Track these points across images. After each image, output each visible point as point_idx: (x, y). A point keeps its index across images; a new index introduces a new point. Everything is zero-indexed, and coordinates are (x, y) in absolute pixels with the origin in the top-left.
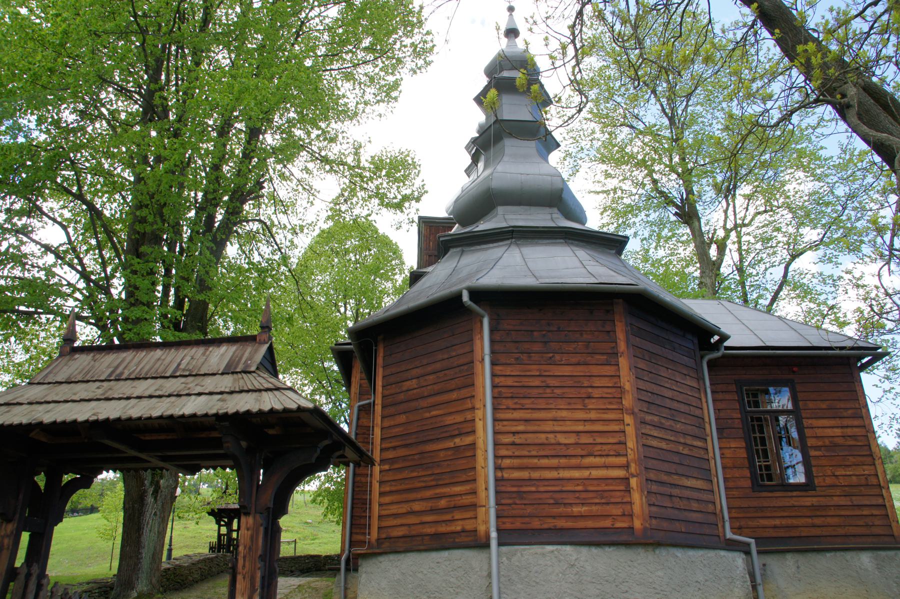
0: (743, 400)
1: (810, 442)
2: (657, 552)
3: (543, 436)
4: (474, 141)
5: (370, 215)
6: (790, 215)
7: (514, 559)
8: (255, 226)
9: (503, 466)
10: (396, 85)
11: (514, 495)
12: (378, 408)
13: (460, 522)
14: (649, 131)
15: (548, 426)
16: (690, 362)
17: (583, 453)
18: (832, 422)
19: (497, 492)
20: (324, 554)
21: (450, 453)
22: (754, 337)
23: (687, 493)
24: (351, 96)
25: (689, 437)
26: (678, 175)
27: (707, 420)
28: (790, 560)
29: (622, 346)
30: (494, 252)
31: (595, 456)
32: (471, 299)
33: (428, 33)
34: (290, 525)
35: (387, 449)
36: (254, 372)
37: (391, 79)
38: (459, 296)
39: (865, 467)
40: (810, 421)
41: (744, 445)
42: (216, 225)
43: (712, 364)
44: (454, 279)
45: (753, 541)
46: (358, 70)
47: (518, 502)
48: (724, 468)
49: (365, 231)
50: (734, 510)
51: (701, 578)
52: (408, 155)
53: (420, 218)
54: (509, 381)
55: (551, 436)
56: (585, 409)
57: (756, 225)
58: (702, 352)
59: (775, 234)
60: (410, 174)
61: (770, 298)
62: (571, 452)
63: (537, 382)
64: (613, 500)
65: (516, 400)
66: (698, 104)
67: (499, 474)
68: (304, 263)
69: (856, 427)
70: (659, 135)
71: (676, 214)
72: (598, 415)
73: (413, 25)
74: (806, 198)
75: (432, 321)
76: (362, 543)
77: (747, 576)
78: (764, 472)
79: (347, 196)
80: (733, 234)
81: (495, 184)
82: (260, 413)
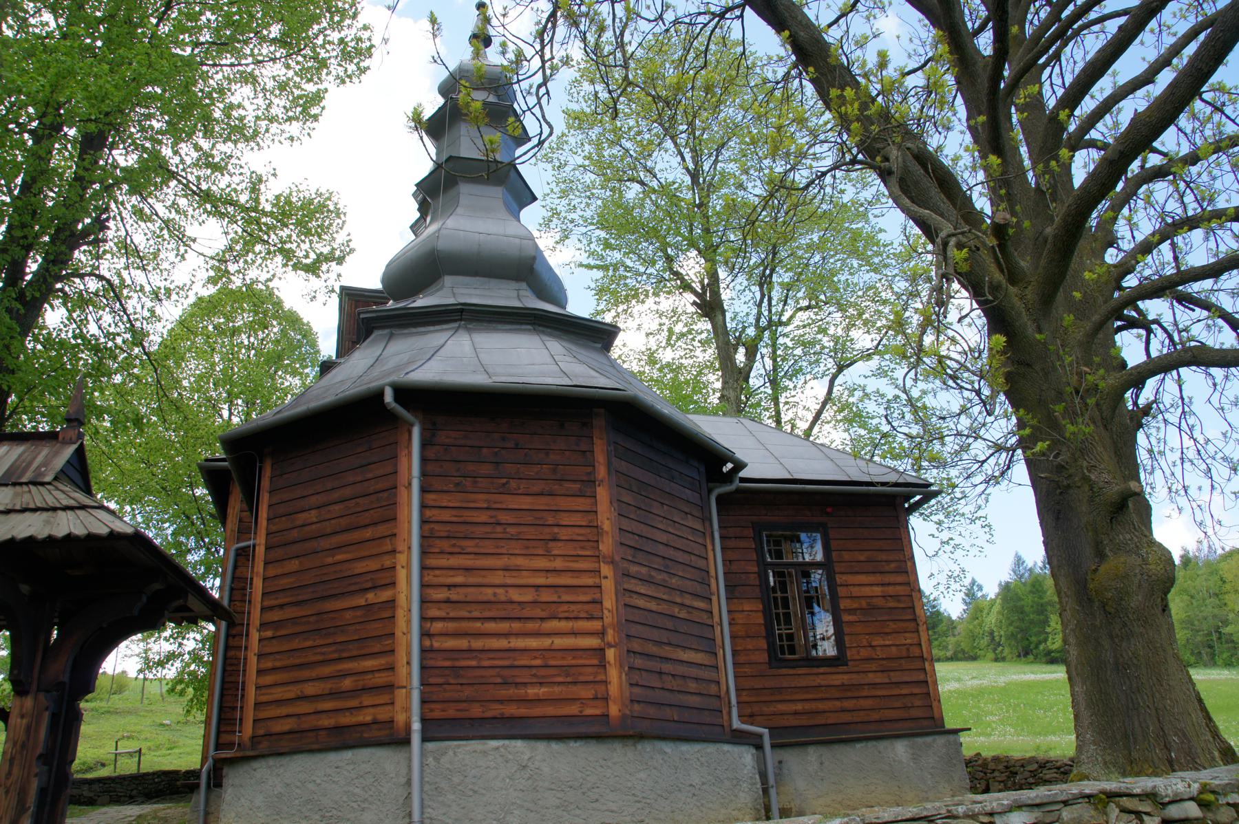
0: (762, 548)
1: (843, 604)
2: (639, 747)
3: (490, 591)
7: (444, 760)
8: (93, 285)
9: (433, 631)
10: (317, 98)
11: (447, 672)
12: (261, 551)
13: (371, 710)
14: (666, 190)
15: (497, 578)
19: (423, 668)
20: (184, 768)
21: (359, 613)
23: (681, 670)
24: (250, 108)
26: (700, 252)
27: (712, 573)
28: (813, 754)
29: (602, 472)
30: (435, 338)
31: (560, 619)
33: (365, 28)
34: (132, 728)
35: (271, 608)
36: (49, 483)
38: (380, 394)
40: (844, 577)
42: (28, 278)
43: (721, 500)
44: (376, 372)
45: (766, 731)
46: (263, 71)
47: (452, 681)
49: (262, 303)
50: (744, 693)
51: (696, 780)
53: (343, 288)
55: (500, 591)
56: (548, 555)
58: (711, 485)
59: (819, 336)
60: (331, 225)
61: (811, 419)
62: (526, 613)
63: (483, 517)
64: (582, 678)
67: (427, 643)
68: (171, 348)
69: (900, 584)
71: (694, 303)
74: (860, 293)
75: (346, 428)
76: (230, 745)
78: (785, 643)
80: (767, 334)
81: (442, 245)
82: (51, 539)
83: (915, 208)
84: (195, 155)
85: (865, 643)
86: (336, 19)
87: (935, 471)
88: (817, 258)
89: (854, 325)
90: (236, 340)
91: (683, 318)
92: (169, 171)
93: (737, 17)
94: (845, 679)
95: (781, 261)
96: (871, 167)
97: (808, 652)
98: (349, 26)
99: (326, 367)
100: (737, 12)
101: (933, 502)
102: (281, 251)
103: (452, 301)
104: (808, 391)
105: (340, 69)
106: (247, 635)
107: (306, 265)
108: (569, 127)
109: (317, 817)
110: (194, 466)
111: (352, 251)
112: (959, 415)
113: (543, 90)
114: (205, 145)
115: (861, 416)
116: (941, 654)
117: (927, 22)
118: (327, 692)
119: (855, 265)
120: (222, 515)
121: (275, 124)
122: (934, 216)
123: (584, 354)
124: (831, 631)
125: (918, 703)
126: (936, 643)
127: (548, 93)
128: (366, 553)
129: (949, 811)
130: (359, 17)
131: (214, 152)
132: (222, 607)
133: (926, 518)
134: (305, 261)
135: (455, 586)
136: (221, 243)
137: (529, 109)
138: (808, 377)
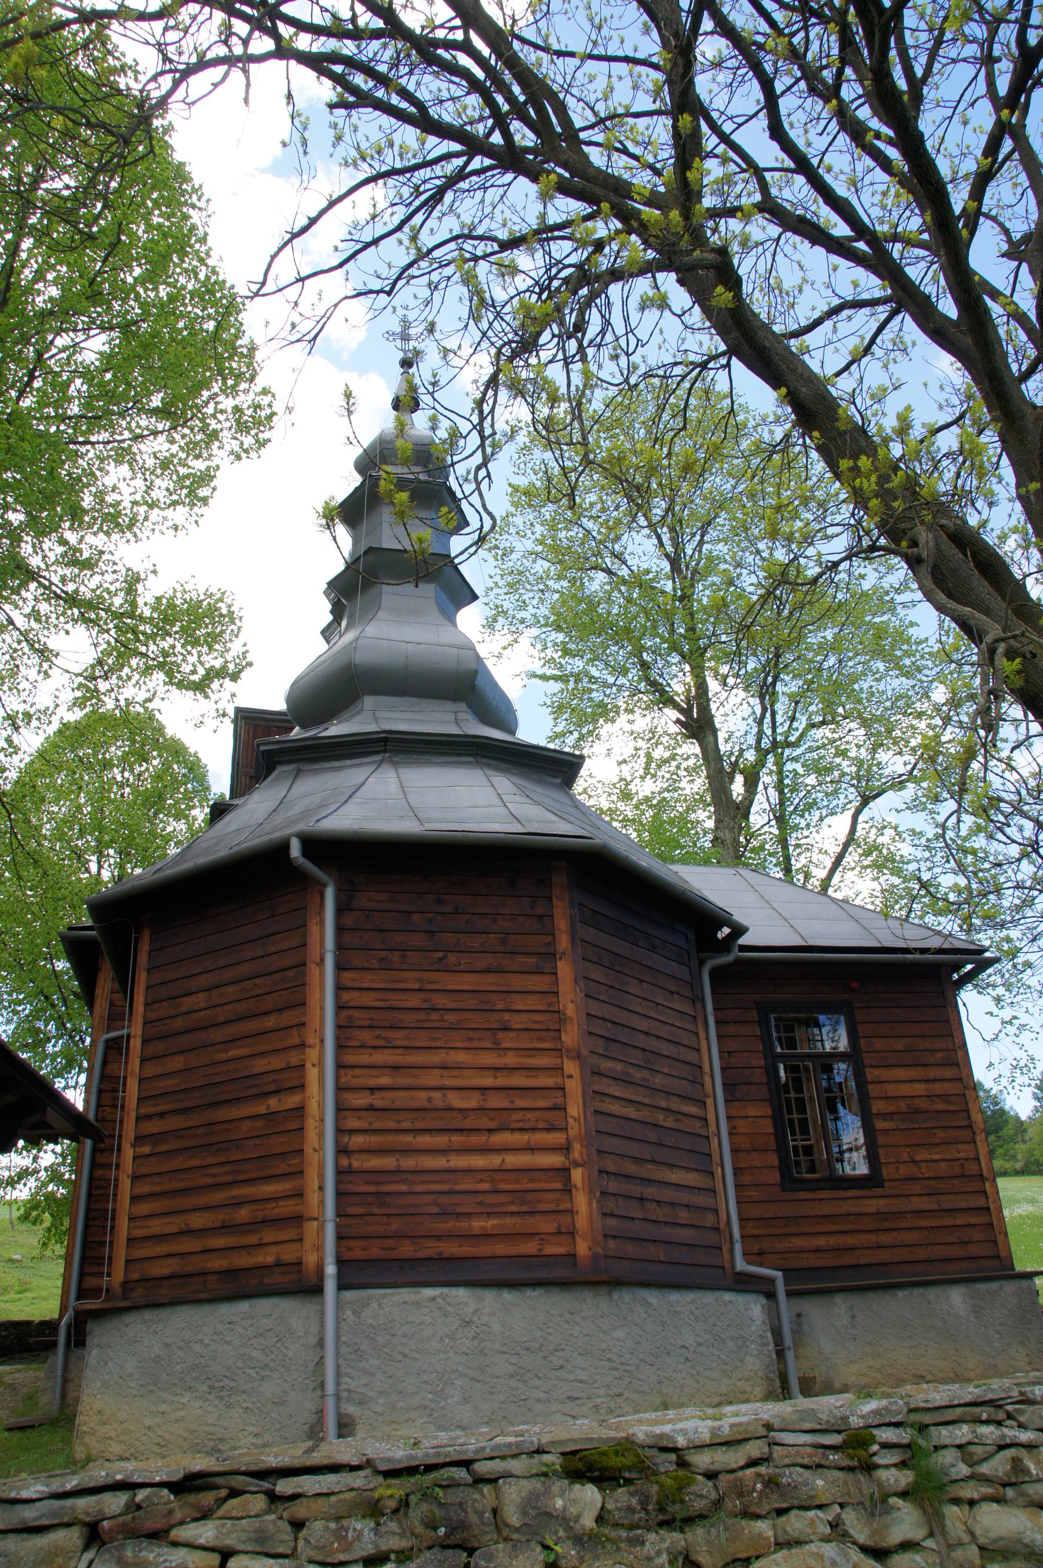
0: (770, 1035)
1: (877, 1107)
2: (616, 1296)
3: (423, 1095)
4: (333, 585)
5: (150, 700)
6: (862, 732)
7: (366, 1314)
10: (206, 478)
12: (136, 1044)
13: (274, 1249)
14: (641, 581)
15: (433, 1079)
16: (682, 972)
17: (492, 1125)
19: (339, 1194)
20: (37, 1319)
21: (258, 1124)
22: (791, 930)
23: (669, 1194)
25: (675, 1098)
26: (683, 657)
27: (706, 1068)
28: (841, 1304)
29: (563, 942)
30: (352, 774)
31: (513, 1130)
32: (305, 853)
35: (149, 1117)
37: (199, 465)
38: (283, 847)
39: (960, 1146)
40: (876, 1072)
41: (769, 1112)
43: (714, 973)
44: (279, 819)
45: (779, 1274)
46: (142, 446)
47: (376, 1211)
48: (734, 1151)
49: (141, 732)
50: (751, 1224)
51: (690, 1340)
52: (221, 600)
53: (238, 710)
54: (368, 999)
56: (497, 1048)
57: (808, 744)
58: (702, 955)
59: (838, 760)
60: (223, 632)
61: (829, 865)
62: (469, 1123)
63: (414, 1001)
64: (541, 1207)
65: (378, 1032)
66: (719, 541)
67: (345, 1162)
70: (654, 588)
71: (678, 721)
72: (519, 1060)
73: (239, 377)
74: (888, 704)
75: (237, 893)
76: (96, 1292)
77: (769, 1335)
78: (802, 1158)
79: (102, 668)
80: (771, 758)
81: (361, 658)
83: (952, 605)
84: (60, 550)
85: (905, 1157)
86: (230, 382)
87: (991, 932)
88: (832, 660)
89: (882, 745)
90: (107, 775)
91: (664, 740)
92: (28, 571)
93: (723, 367)
94: (880, 1205)
95: (786, 666)
96: (896, 553)
97: (831, 1168)
98: (246, 392)
99: (219, 810)
100: (723, 361)
101: (990, 971)
102: (161, 666)
103: (372, 728)
104: (825, 830)
105: (234, 442)
106: (119, 1150)
107: (194, 682)
108: (516, 505)
109: (205, 1388)
110: (54, 934)
111: (250, 664)
112: (1019, 860)
113: (483, 473)
114: (72, 537)
115: (893, 861)
116: (1008, 1165)
117: (959, 365)
118: (219, 1225)
119: (882, 669)
120: (88, 994)
121: (156, 511)
122: (977, 614)
123: (539, 791)
124: (862, 1140)
125: (977, 1236)
126: (1001, 1151)
127: (489, 476)
128: (268, 1048)
129: (1022, 1394)
130: (258, 379)
131: (83, 546)
132: (89, 1123)
133: (981, 989)
134: (192, 678)
135: (379, 1089)
136: (90, 657)
137: (466, 497)
138: (824, 812)
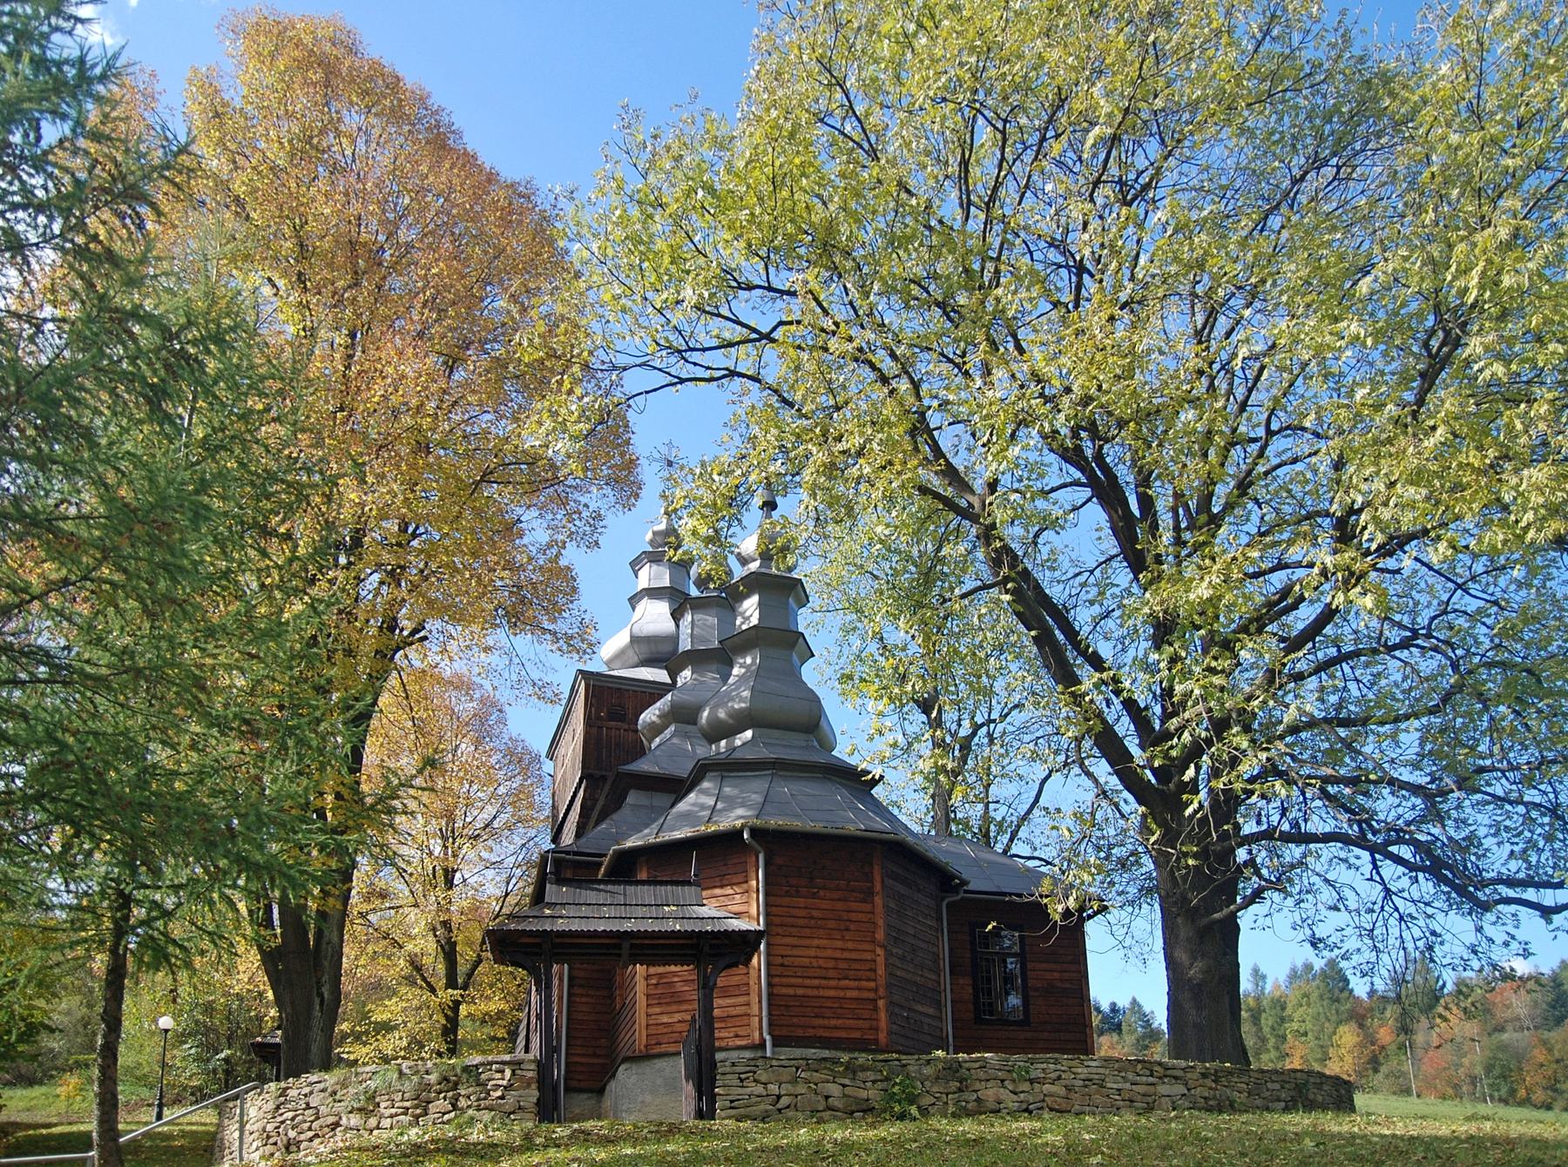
18: (1054, 966)
29: (878, 887)
56: (843, 939)
94: (1029, 1035)
